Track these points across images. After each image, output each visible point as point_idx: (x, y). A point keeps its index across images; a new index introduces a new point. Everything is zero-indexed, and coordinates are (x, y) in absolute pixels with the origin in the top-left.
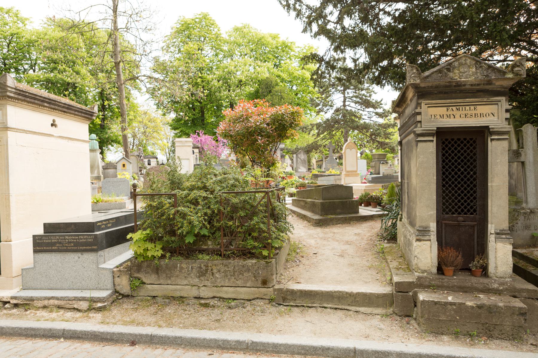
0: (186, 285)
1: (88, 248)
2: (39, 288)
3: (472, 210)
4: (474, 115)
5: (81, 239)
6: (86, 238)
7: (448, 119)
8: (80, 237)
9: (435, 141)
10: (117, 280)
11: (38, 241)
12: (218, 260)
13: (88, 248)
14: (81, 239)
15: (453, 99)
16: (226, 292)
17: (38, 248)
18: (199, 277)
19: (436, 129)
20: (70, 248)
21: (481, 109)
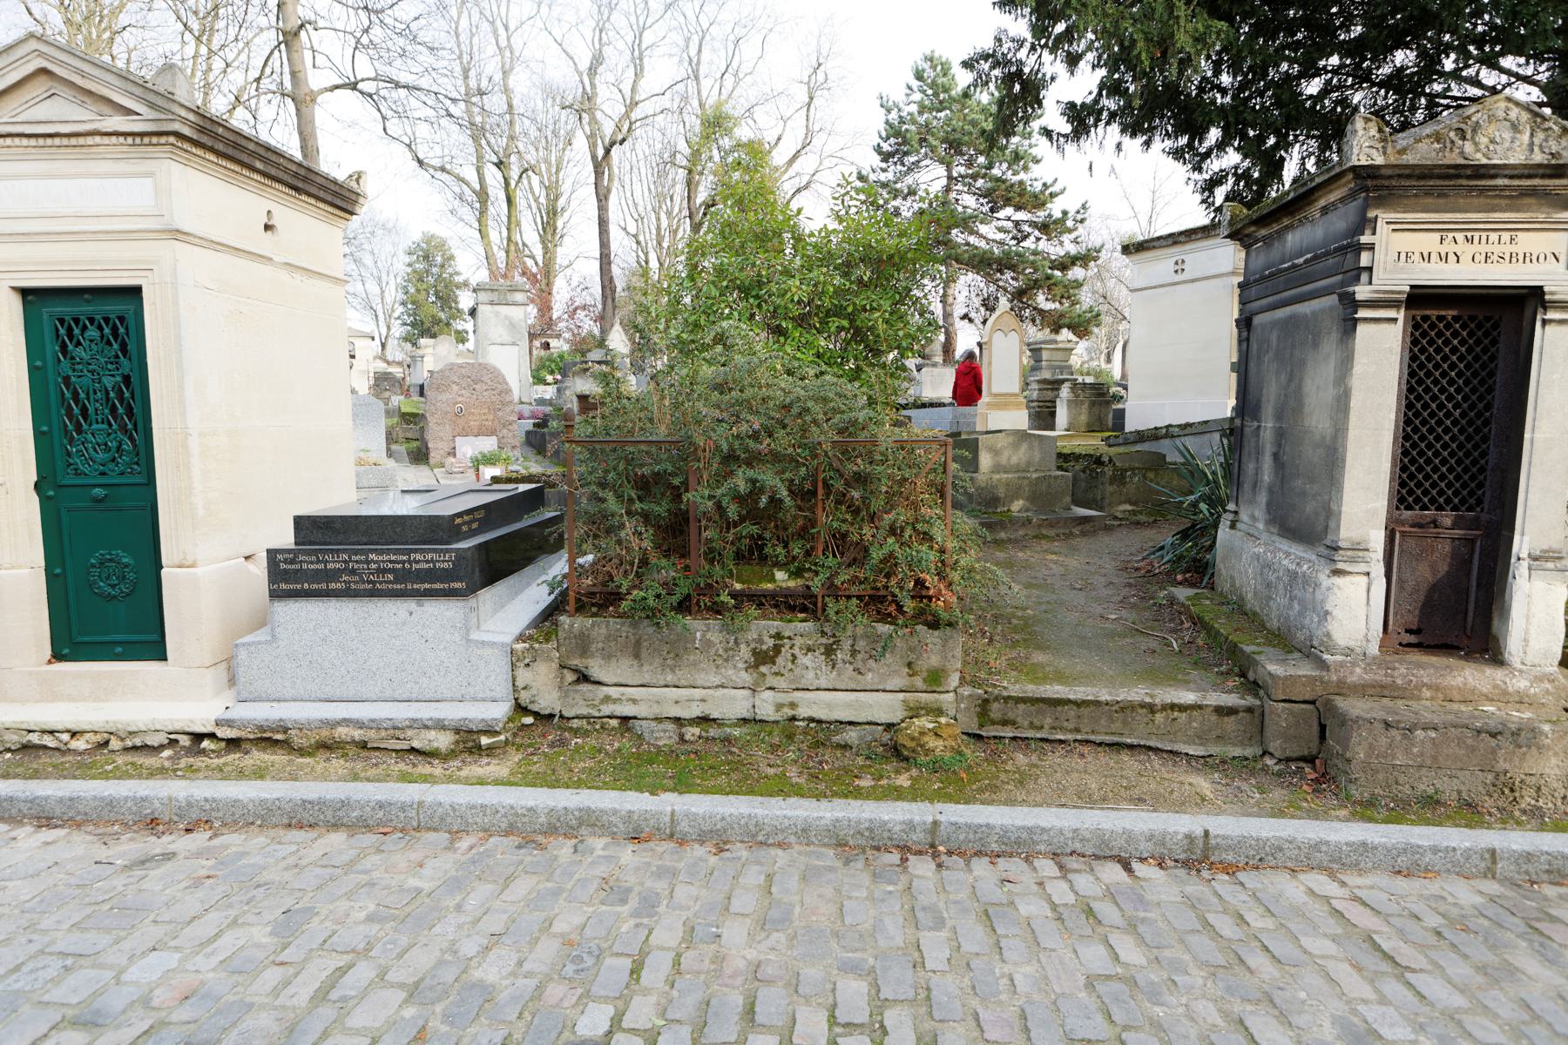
1: (438, 586)
2: (287, 696)
3: (1472, 501)
4: (1507, 257)
5: (417, 562)
6: (432, 561)
7: (1442, 265)
8: (413, 556)
9: (1401, 322)
10: (524, 676)
11: (283, 566)
12: (801, 628)
13: (438, 586)
14: (417, 562)
15: (1459, 211)
17: (284, 586)
18: (756, 666)
19: (1407, 289)
20: (384, 586)
21: (1529, 242)
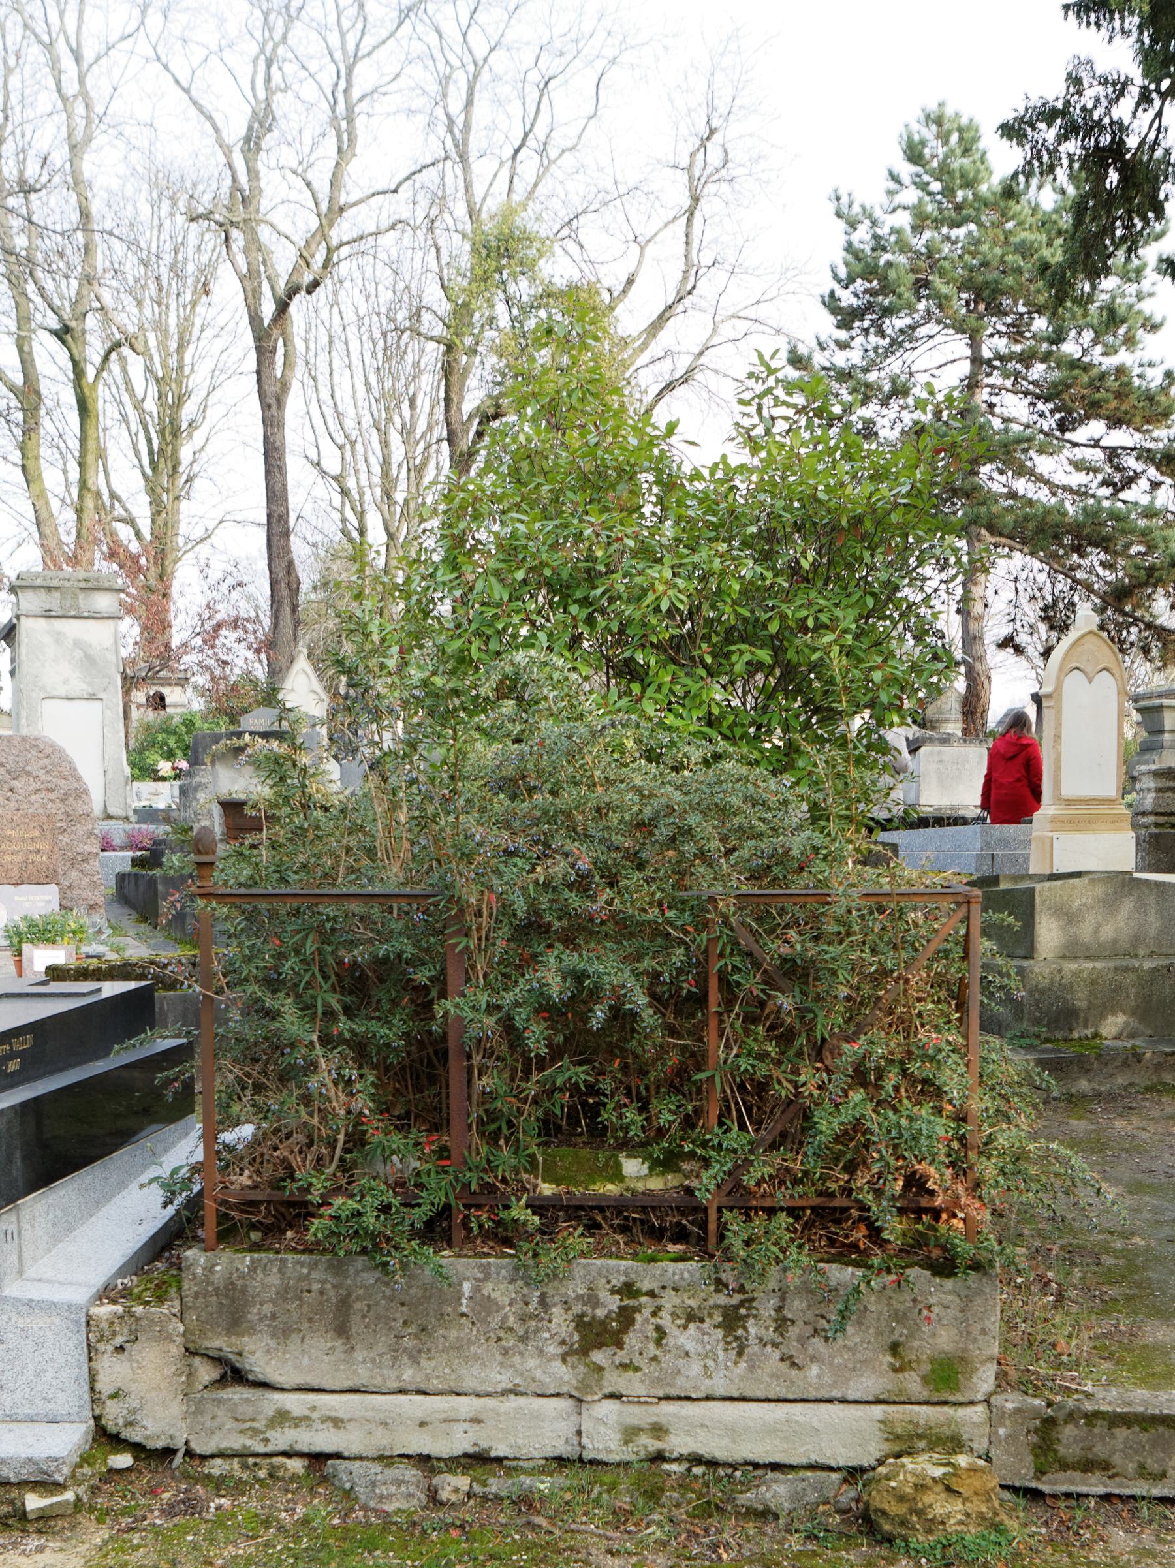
0: (505, 1393)
12: (675, 1273)
16: (732, 1431)
